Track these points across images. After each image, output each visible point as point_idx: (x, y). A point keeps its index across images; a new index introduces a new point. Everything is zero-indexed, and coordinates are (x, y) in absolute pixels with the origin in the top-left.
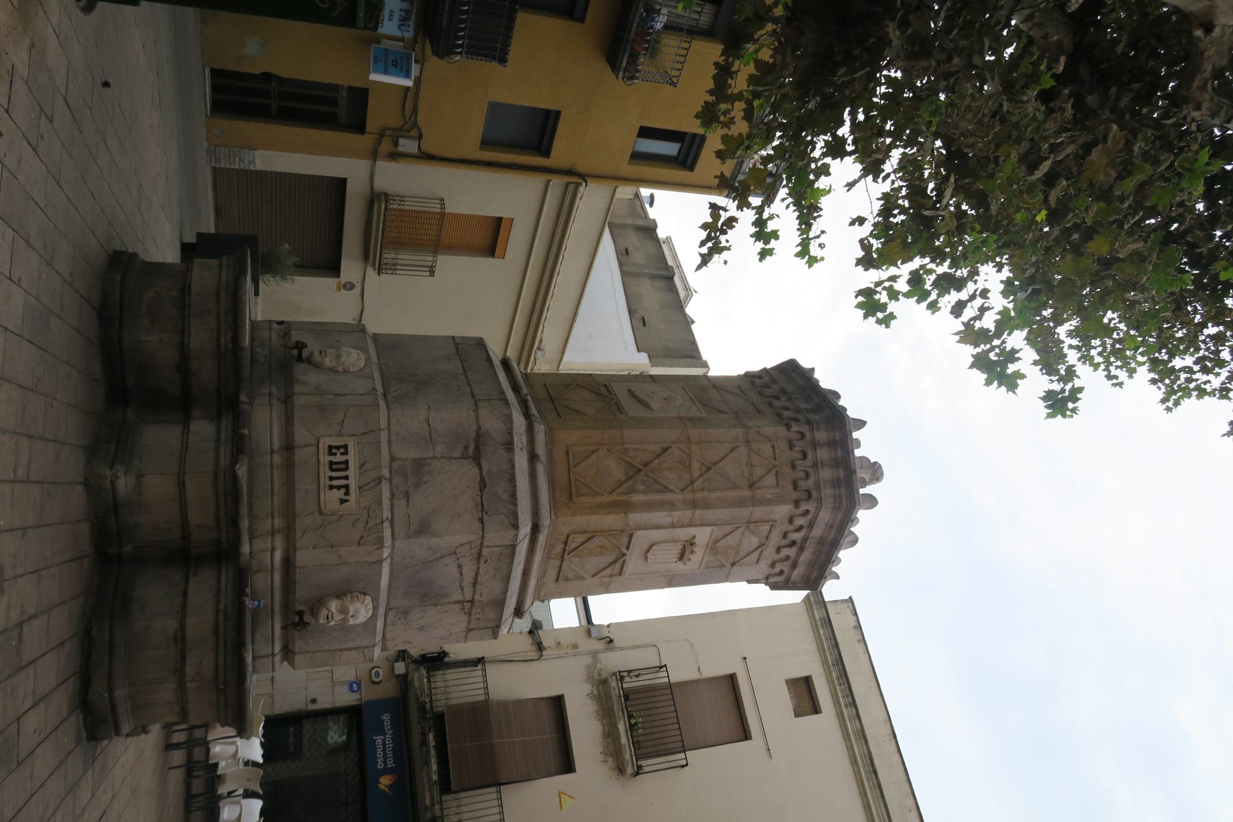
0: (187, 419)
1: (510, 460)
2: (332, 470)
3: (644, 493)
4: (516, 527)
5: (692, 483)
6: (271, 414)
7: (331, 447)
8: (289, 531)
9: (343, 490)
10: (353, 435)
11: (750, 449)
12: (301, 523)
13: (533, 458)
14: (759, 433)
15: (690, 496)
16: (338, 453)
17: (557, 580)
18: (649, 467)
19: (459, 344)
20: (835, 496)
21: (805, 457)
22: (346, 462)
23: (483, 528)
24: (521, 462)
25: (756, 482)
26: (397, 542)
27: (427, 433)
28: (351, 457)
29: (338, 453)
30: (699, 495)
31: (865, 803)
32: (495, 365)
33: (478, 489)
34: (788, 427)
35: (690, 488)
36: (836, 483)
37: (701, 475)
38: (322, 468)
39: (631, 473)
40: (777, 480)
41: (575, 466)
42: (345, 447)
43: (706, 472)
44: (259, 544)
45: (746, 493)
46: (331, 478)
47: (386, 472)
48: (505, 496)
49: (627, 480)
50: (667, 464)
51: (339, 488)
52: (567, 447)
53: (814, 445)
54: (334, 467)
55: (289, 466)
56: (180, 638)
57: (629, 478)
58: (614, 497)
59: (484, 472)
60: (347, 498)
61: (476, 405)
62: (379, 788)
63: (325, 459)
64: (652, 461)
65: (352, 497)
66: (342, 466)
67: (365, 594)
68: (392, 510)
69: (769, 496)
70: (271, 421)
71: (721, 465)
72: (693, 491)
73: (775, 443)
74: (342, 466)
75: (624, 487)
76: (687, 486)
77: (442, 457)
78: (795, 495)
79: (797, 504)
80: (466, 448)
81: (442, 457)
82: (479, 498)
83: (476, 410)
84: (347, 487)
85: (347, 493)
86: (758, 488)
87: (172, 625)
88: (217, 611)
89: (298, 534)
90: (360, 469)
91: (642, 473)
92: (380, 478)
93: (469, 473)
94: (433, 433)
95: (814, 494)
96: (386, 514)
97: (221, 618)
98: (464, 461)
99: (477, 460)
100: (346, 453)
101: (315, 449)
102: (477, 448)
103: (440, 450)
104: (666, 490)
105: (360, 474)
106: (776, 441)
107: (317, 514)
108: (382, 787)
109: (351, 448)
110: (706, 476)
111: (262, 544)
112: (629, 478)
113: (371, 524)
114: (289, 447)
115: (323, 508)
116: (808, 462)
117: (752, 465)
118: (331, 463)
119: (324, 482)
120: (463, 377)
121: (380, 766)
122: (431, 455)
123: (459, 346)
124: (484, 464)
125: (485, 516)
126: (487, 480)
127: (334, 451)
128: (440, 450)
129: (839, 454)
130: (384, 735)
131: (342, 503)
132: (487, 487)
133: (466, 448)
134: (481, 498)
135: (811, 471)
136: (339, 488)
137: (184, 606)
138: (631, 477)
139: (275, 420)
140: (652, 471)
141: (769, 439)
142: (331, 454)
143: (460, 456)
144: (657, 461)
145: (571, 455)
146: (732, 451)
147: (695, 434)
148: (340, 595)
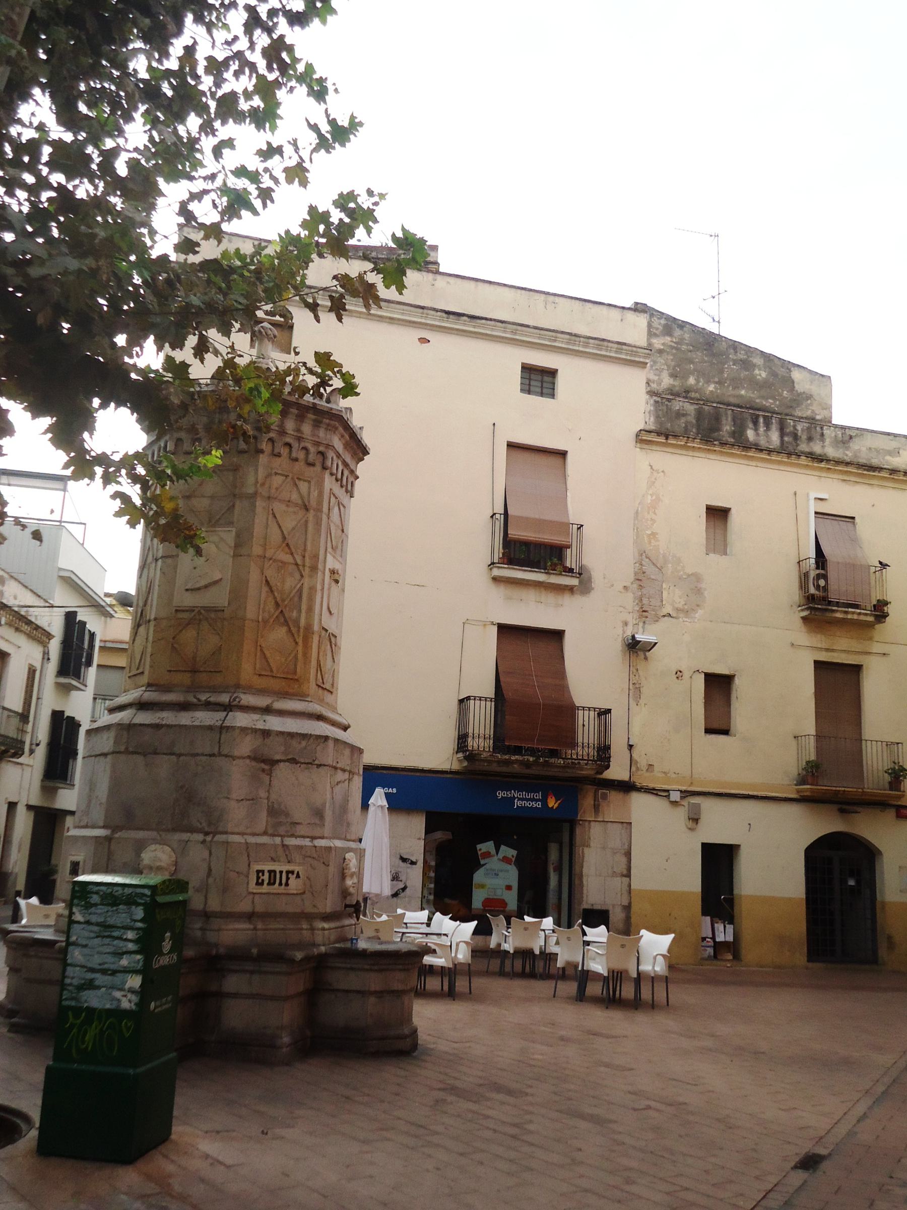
0: (220, 995)
1: (277, 735)
2: (274, 883)
3: (300, 611)
4: (326, 738)
5: (297, 564)
6: (227, 930)
7: (257, 884)
8: (310, 917)
9: (290, 875)
10: (249, 865)
11: (276, 498)
12: (309, 909)
13: (267, 710)
14: (263, 484)
15: (307, 569)
16: (262, 878)
17: (331, 693)
18: (280, 602)
19: (127, 748)
20: (326, 429)
21: (289, 445)
22: (270, 872)
23: (325, 765)
24: (275, 723)
25: (304, 502)
26: (326, 835)
27: (248, 802)
28: (267, 867)
29: (262, 878)
30: (307, 564)
31: (388, 320)
32: (157, 721)
33: (294, 765)
34: (262, 451)
35: (301, 568)
36: (317, 424)
37: (292, 554)
38: (272, 891)
39: (282, 620)
40: (305, 481)
41: (272, 671)
42: (258, 872)
43: (289, 548)
44: (319, 939)
45: (311, 515)
46: (280, 884)
47: (278, 840)
48: (304, 743)
49: (288, 625)
50: (279, 584)
51: (288, 879)
52: (255, 674)
53: (282, 432)
54: (272, 881)
55: (266, 916)
56: (380, 994)
57: (286, 623)
58: (300, 641)
59: (283, 758)
60: (296, 873)
61: (226, 756)
62: (556, 808)
63: (265, 888)
64: (275, 598)
65: (296, 868)
66: (272, 874)
67: (345, 859)
68: (304, 837)
69: (316, 493)
70: (231, 930)
71: (285, 532)
72: (304, 566)
73: (274, 471)
74: (272, 874)
75: (294, 630)
76: (299, 569)
77: (268, 791)
78: (318, 468)
79: (324, 468)
80: (263, 770)
81: (268, 791)
82: (302, 766)
83: (234, 758)
84: (288, 872)
85: (292, 872)
86: (309, 502)
87: (372, 1000)
88: (371, 970)
89: (316, 911)
90: (275, 861)
91: (284, 610)
92: (283, 845)
93: (283, 771)
94: (248, 798)
95: (321, 449)
96: (307, 842)
97: (376, 967)
98: (274, 774)
99: (273, 763)
100: (263, 872)
101: (257, 897)
102: (264, 761)
103: (263, 794)
104: (300, 592)
105: (279, 861)
106: (272, 469)
107: (304, 896)
108: (556, 805)
109: (260, 868)
110: (293, 550)
111: (319, 937)
112: (286, 623)
113: (315, 855)
114: (250, 916)
115: (299, 892)
116: (295, 445)
117: (289, 501)
118: (269, 884)
119: (282, 889)
120: (182, 758)
121: (539, 805)
122: (266, 801)
123: (131, 749)
124: (277, 757)
125: (316, 762)
126: (290, 757)
127: (260, 881)
128: (263, 794)
129: (296, 412)
130: (514, 798)
131: (299, 877)
132: (295, 757)
133: (263, 770)
134: (302, 763)
135: (302, 445)
136: (288, 879)
137: (358, 992)
138: (286, 621)
139: (231, 927)
140: (283, 601)
141: (269, 476)
142: (262, 884)
143: (269, 777)
144: (276, 594)
145: (263, 673)
146: (275, 517)
147: (257, 550)
148: (343, 877)
